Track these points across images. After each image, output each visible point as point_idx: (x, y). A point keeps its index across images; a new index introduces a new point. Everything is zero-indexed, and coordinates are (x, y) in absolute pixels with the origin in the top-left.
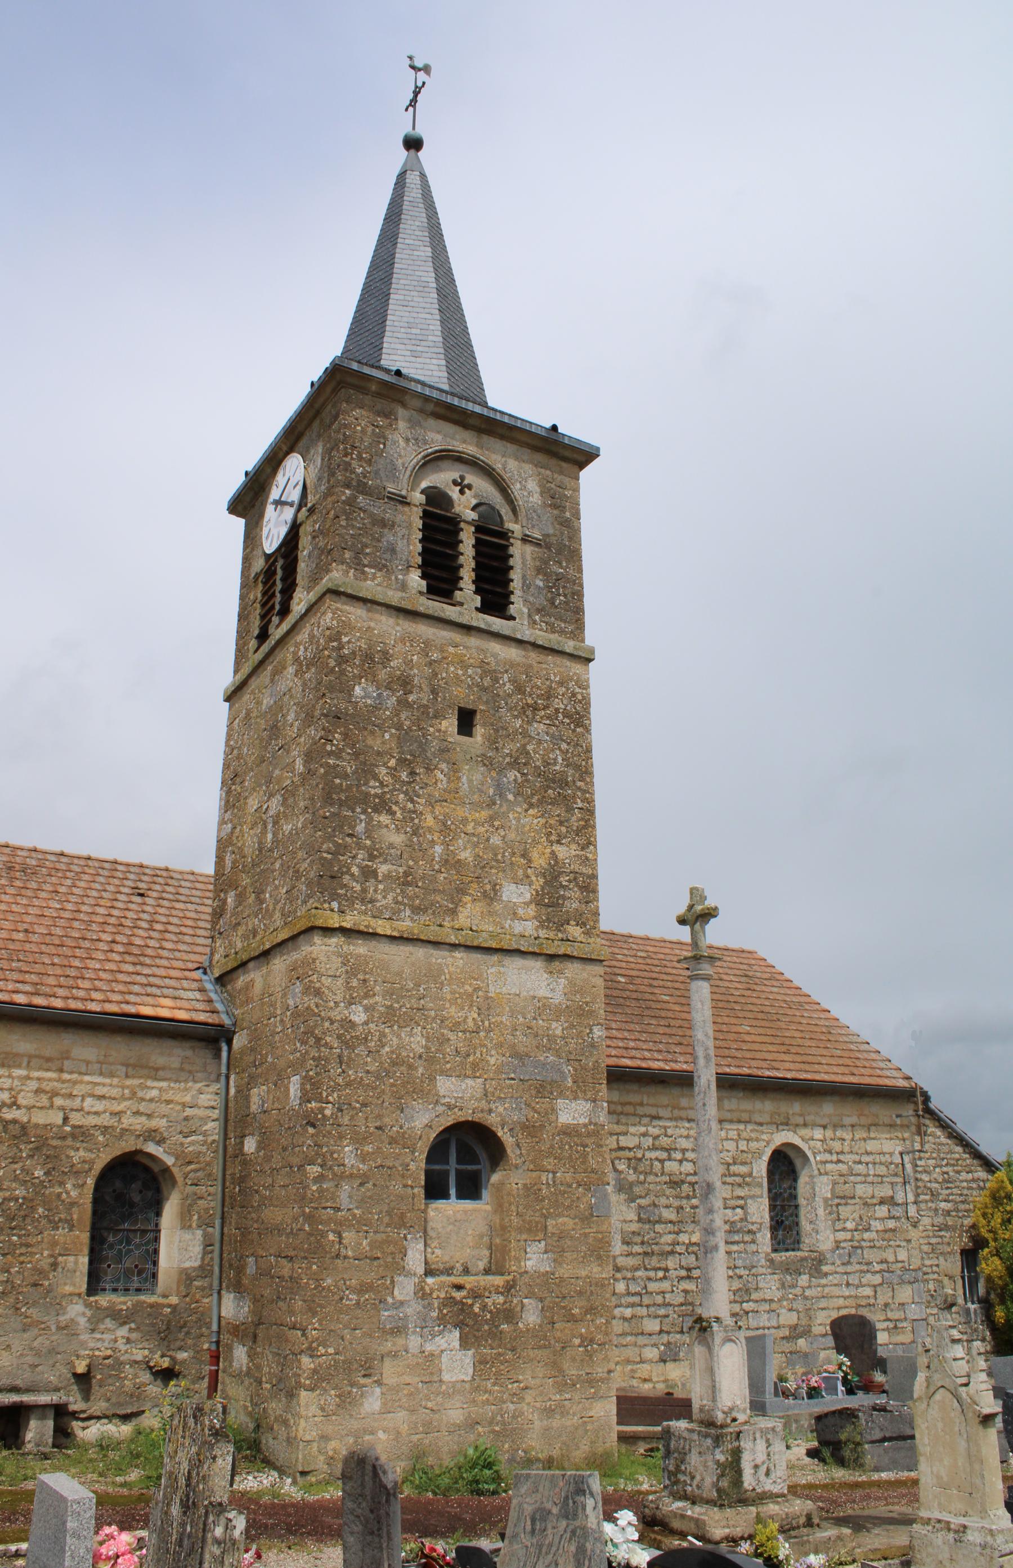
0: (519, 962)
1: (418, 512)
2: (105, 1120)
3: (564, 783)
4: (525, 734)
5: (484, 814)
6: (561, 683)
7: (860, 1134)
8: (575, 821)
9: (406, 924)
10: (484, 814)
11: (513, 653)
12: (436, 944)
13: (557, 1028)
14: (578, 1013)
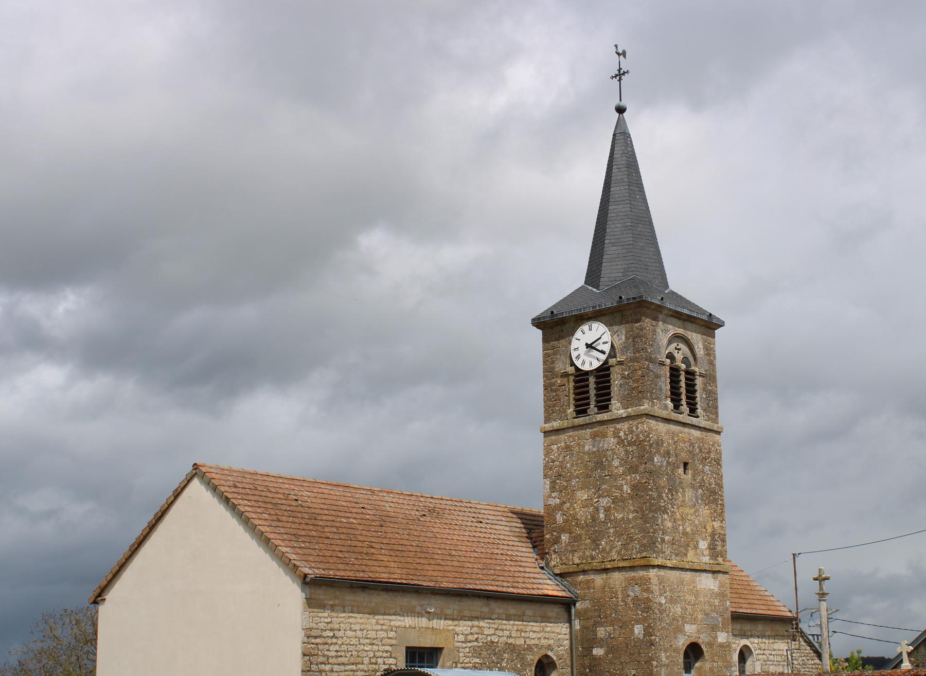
0: (704, 575)
1: (668, 368)
2: (536, 642)
3: (715, 493)
4: (703, 472)
5: (693, 510)
6: (713, 445)
7: (771, 641)
8: (719, 511)
9: (674, 562)
10: (693, 510)
11: (696, 433)
12: (682, 569)
13: (717, 602)
14: (722, 595)
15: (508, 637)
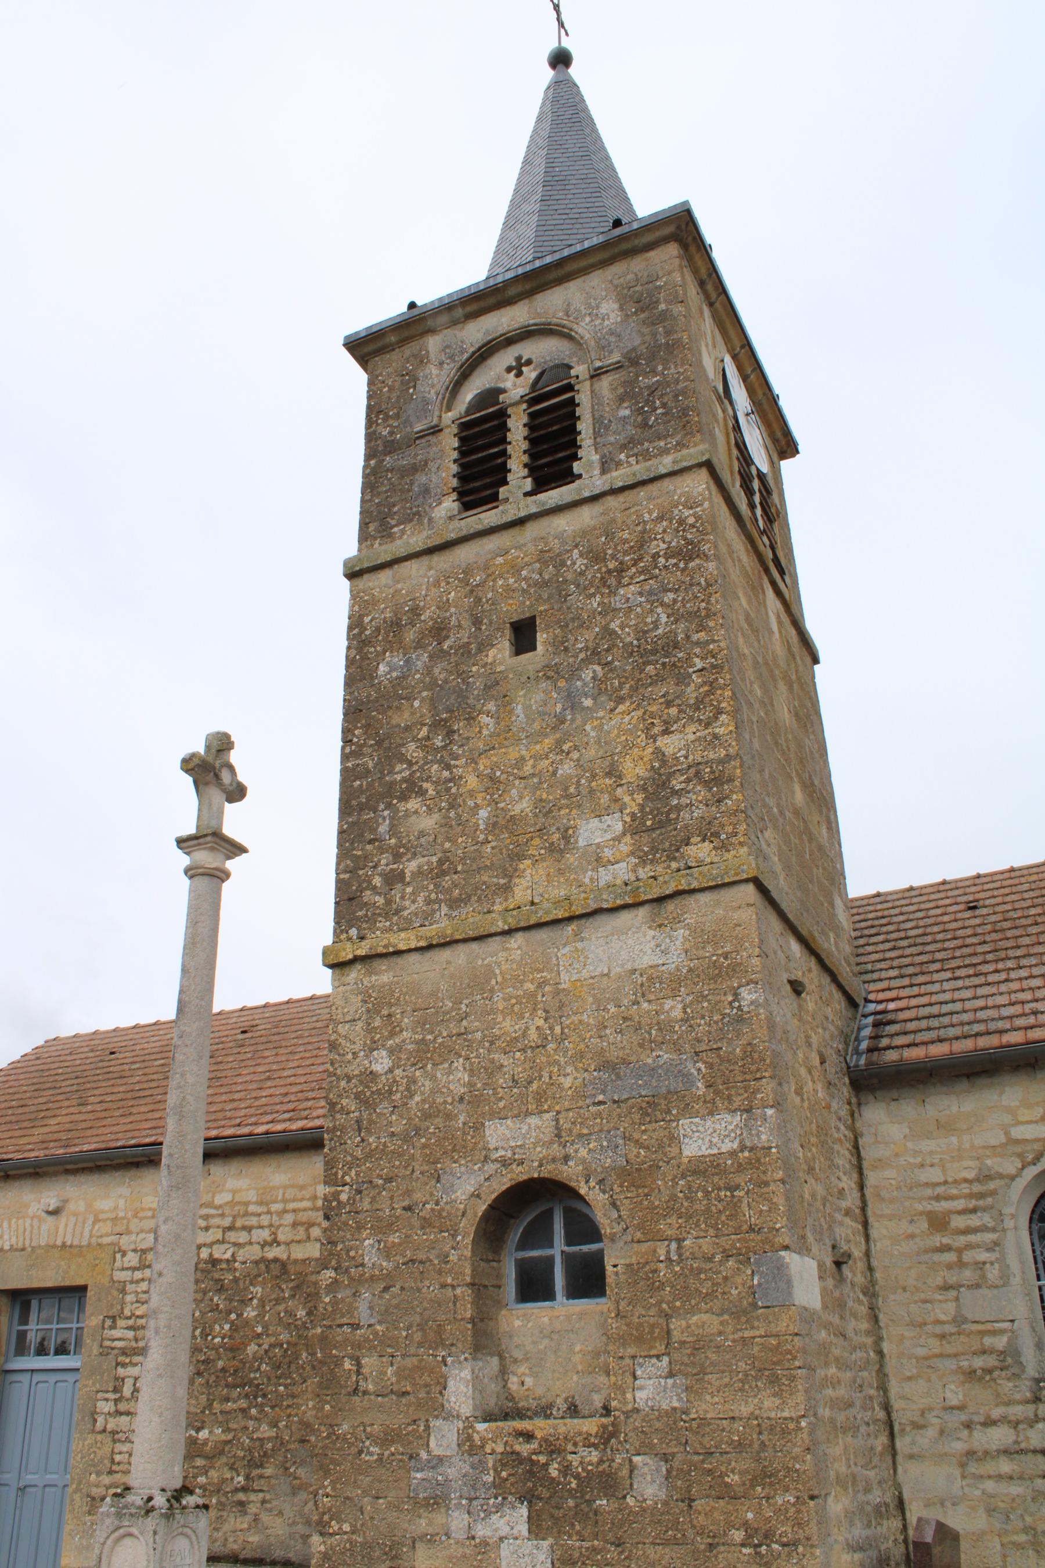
15: (264, 1245)
